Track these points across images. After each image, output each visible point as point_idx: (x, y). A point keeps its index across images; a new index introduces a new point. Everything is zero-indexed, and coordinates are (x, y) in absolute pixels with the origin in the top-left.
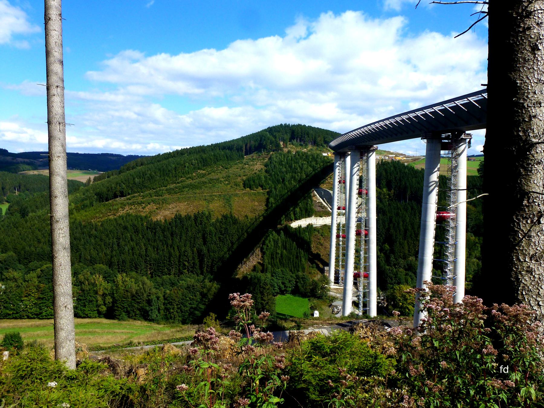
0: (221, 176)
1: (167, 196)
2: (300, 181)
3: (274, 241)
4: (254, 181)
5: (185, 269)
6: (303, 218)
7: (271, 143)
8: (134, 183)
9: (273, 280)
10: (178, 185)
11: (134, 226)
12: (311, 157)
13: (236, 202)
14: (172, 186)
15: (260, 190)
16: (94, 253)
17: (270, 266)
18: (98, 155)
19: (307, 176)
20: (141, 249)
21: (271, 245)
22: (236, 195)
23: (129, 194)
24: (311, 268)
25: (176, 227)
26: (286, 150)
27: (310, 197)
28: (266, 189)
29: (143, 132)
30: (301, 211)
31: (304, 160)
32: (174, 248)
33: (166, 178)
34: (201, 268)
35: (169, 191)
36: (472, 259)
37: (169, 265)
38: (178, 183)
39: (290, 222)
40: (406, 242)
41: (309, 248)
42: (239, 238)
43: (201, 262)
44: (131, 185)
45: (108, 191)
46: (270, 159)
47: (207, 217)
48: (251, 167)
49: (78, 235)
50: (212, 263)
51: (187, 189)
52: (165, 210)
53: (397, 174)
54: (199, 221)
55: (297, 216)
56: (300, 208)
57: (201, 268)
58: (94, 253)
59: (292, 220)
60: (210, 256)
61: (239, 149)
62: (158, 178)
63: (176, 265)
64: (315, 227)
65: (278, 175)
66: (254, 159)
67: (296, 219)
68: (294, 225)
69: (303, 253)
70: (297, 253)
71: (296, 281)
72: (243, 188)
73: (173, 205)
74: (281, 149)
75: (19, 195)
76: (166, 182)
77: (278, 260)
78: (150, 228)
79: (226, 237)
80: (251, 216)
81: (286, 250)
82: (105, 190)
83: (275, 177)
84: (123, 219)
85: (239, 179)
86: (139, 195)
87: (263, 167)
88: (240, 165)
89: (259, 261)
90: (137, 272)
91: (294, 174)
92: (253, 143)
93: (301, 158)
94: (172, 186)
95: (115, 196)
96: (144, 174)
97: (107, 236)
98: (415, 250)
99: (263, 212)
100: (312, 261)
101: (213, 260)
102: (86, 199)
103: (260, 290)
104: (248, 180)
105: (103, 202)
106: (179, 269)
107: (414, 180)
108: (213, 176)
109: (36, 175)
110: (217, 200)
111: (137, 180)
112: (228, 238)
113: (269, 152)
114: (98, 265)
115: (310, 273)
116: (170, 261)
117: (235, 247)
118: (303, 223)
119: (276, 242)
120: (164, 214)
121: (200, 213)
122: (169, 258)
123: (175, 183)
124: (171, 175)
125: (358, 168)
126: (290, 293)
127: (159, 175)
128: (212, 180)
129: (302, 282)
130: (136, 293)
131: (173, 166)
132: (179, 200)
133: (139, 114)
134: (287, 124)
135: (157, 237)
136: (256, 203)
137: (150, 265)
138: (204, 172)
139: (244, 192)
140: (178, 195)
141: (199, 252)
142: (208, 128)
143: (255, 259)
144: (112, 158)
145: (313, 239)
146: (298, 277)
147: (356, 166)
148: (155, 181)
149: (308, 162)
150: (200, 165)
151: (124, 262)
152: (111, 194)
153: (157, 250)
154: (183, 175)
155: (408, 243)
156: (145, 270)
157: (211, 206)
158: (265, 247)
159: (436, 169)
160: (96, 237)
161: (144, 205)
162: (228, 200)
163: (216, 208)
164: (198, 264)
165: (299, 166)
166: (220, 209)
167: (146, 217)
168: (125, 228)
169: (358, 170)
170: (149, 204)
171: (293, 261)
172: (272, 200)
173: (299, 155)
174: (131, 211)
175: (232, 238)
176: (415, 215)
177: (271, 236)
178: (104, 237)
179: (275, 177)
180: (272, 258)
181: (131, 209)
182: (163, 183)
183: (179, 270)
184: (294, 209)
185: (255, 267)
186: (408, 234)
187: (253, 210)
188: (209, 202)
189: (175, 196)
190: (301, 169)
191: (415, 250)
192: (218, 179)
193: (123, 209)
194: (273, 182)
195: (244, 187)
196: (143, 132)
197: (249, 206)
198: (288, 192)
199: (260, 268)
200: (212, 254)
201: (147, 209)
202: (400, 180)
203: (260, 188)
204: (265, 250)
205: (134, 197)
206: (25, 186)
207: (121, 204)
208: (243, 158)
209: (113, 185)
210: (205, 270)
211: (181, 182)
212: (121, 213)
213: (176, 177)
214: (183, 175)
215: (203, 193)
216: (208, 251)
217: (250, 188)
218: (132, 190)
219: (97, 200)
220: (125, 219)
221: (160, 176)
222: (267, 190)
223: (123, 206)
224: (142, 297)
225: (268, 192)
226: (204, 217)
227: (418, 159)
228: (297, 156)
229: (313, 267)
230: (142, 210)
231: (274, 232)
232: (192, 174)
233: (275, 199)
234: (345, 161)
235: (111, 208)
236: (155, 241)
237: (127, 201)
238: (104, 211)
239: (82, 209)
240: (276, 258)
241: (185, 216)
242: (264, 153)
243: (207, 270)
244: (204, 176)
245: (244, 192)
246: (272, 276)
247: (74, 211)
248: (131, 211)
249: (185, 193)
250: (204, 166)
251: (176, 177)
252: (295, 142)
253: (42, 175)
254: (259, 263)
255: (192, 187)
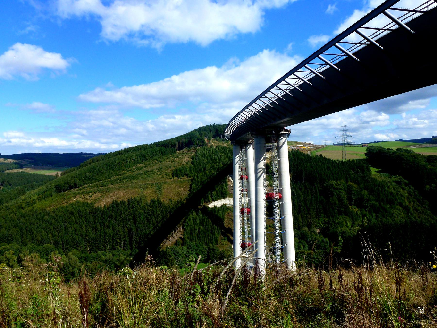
0: (155, 168)
1: (110, 186)
2: (218, 169)
3: (193, 218)
4: (180, 172)
5: (118, 245)
6: (219, 199)
7: (198, 139)
8: (86, 177)
9: (188, 251)
10: (120, 176)
11: (79, 211)
12: (228, 150)
13: (165, 189)
14: (115, 178)
15: (185, 178)
16: (44, 235)
17: (188, 240)
18: (74, 154)
19: (224, 165)
20: (82, 229)
21: (191, 223)
22: (165, 183)
23: (81, 186)
24: (223, 240)
25: (112, 211)
26: (209, 145)
27: (225, 183)
28: (190, 177)
29: (117, 136)
30: (217, 193)
31: (223, 153)
32: (109, 229)
33: (111, 171)
34: (131, 244)
35: (112, 182)
36: (355, 227)
37: (104, 242)
38: (120, 175)
39: (208, 203)
40: (300, 216)
41: (223, 224)
42: (163, 218)
43: (131, 239)
44: (83, 179)
45: (65, 183)
46: (196, 153)
47: (138, 202)
48: (181, 160)
49: (33, 220)
50: (140, 239)
51: (126, 180)
52: (107, 197)
53: (295, 160)
54: (131, 206)
55: (214, 198)
56: (217, 191)
57: (131, 244)
58: (44, 235)
59: (209, 202)
60: (138, 234)
61: (173, 146)
62: (105, 172)
63: (110, 242)
64: (228, 207)
65: (200, 166)
66: (183, 154)
67: (213, 200)
68: (211, 205)
69: (216, 228)
70: (212, 229)
71: (208, 252)
72: (171, 177)
73: (114, 193)
74: (206, 145)
75: (3, 189)
76: (111, 175)
77: (196, 235)
78: (92, 213)
79: (152, 218)
80: (175, 199)
81: (203, 226)
82: (63, 183)
83: (198, 167)
84: (72, 206)
85: (170, 170)
86: (89, 186)
87: (190, 159)
88: (172, 159)
89: (181, 236)
90: (77, 249)
91: (213, 164)
92: (184, 140)
93: (220, 151)
94: (115, 178)
95: (71, 188)
96: (94, 168)
97: (57, 220)
98: (308, 222)
99: (187, 196)
100: (224, 234)
101: (140, 238)
102: (47, 191)
103: (165, 261)
104: (176, 170)
105: (60, 192)
106: (113, 245)
107: (308, 165)
108: (149, 168)
109: (19, 172)
110: (150, 188)
111: (87, 174)
112: (153, 219)
113: (196, 147)
114: (47, 244)
115: (222, 245)
116: (105, 239)
117: (160, 225)
118: (218, 203)
119: (195, 220)
120: (104, 202)
121: (133, 199)
122: (105, 237)
123: (118, 175)
124: (115, 169)
125: (239, 158)
126: (203, 262)
127: (106, 169)
128: (147, 171)
129: (212, 252)
130: (63, 267)
131: (118, 161)
132: (119, 189)
133: (113, 123)
134: (216, 124)
135: (97, 220)
136: (182, 189)
137: (89, 243)
138: (142, 165)
139: (172, 180)
140: (119, 185)
141: (130, 230)
142: (165, 131)
143: (178, 235)
144: (85, 156)
145: (226, 216)
146: (209, 248)
147: (237, 157)
148: (103, 174)
149: (225, 154)
150: (139, 160)
151: (67, 241)
152: (67, 186)
153: (96, 230)
154: (125, 169)
155: (301, 216)
156: (85, 247)
157: (145, 193)
158: (186, 224)
159: (262, 159)
160: (47, 221)
161: (91, 194)
162: (159, 187)
163: (149, 194)
164: (128, 241)
165: (218, 158)
166: (152, 195)
167: (91, 204)
168: (72, 213)
169: (239, 160)
170: (95, 193)
171: (208, 235)
172: (194, 186)
173: (219, 149)
174: (80, 199)
175: (158, 218)
176: (308, 193)
177: (191, 215)
178: (53, 221)
179: (198, 167)
180: (191, 233)
181: (80, 198)
182: (108, 176)
183: (113, 246)
184: (212, 192)
185: (176, 241)
186: (302, 208)
187: (179, 195)
188: (143, 189)
189: (117, 186)
190: (220, 160)
191: (308, 222)
192: (152, 171)
193: (75, 198)
194: (196, 172)
195: (173, 176)
196: (117, 136)
197: (175, 192)
198: (208, 178)
199: (181, 242)
200: (139, 232)
201: (93, 197)
202: (297, 165)
203: (185, 176)
204: (185, 227)
205: (84, 188)
206: (8, 182)
207: (74, 194)
208: (175, 153)
209: (69, 179)
210: (134, 246)
211: (123, 174)
212: (73, 201)
213: (119, 170)
214: (125, 169)
215: (139, 182)
216: (137, 230)
217: (178, 177)
218: (84, 182)
219: (55, 191)
220: (74, 206)
221: (107, 170)
222: (192, 178)
223: (75, 195)
224: (67, 270)
225: (191, 179)
226: (135, 202)
227: (320, 148)
228: (217, 150)
229: (225, 240)
230: (89, 198)
231: (194, 213)
232: (132, 167)
233: (196, 185)
234: (246, 153)
235: (65, 197)
236: (95, 223)
237: (79, 192)
238: (59, 200)
239: (44, 199)
240: (194, 233)
241: (153, 201)
242: (192, 148)
243: (135, 245)
244: (141, 168)
245: (172, 180)
246: (188, 248)
247: (37, 201)
248: (80, 199)
249: (125, 183)
250: (143, 160)
251: (119, 170)
252: (218, 138)
253: (25, 172)
254: (180, 238)
255: (131, 178)
